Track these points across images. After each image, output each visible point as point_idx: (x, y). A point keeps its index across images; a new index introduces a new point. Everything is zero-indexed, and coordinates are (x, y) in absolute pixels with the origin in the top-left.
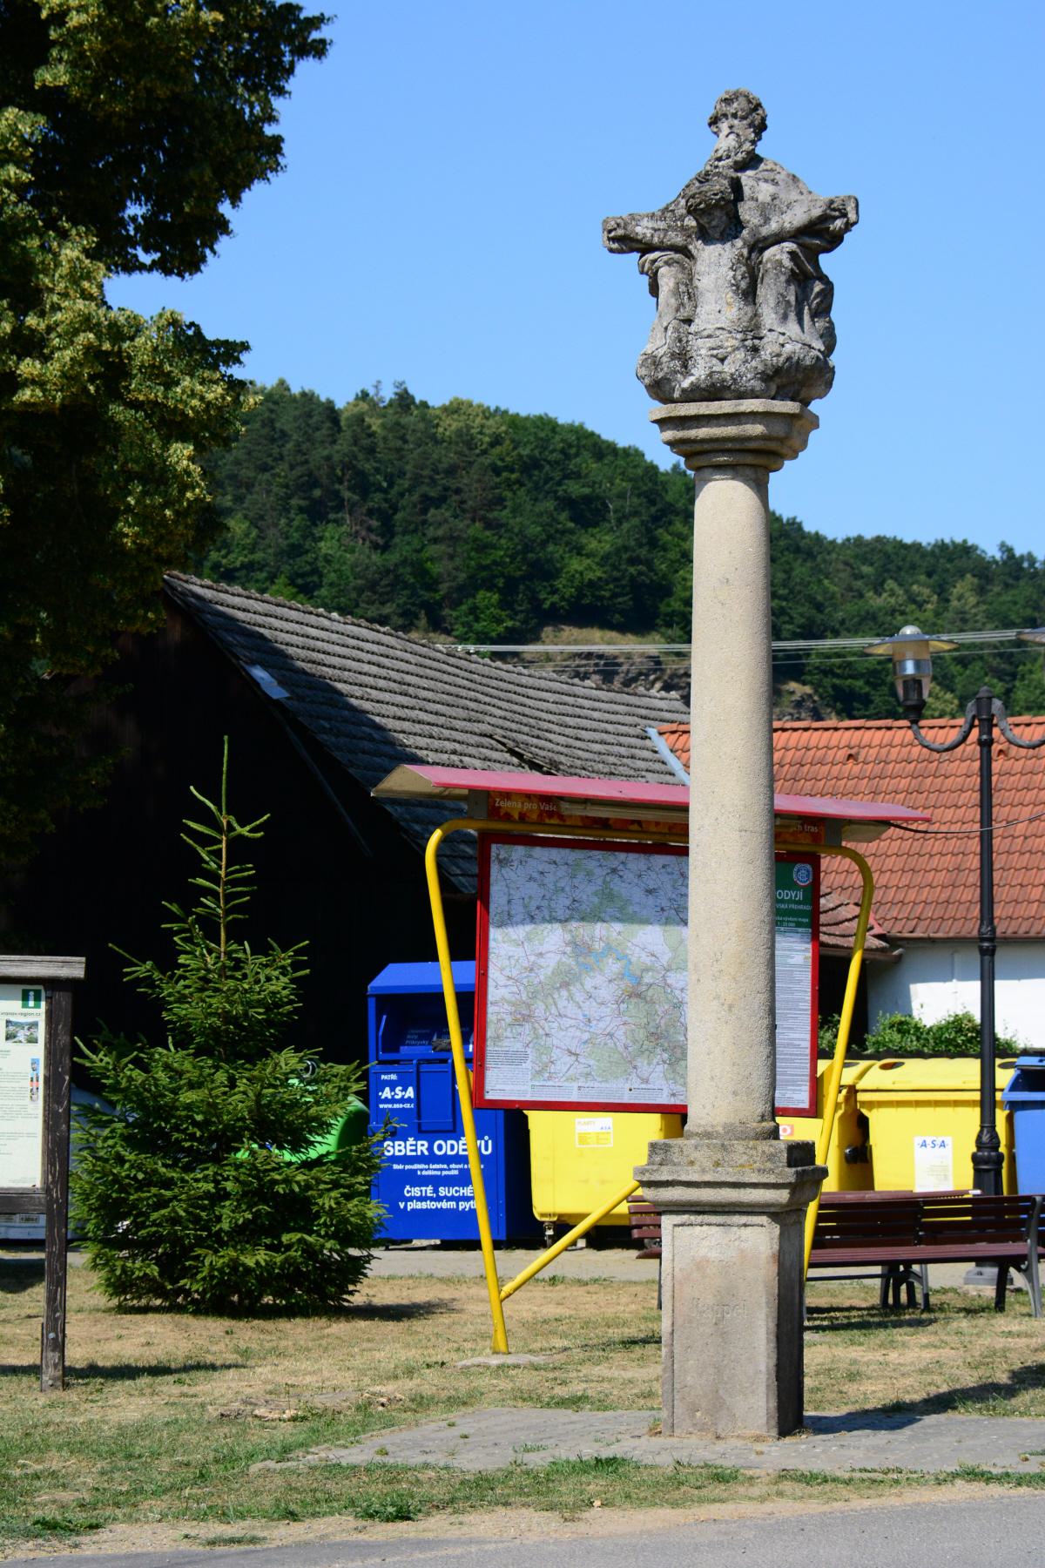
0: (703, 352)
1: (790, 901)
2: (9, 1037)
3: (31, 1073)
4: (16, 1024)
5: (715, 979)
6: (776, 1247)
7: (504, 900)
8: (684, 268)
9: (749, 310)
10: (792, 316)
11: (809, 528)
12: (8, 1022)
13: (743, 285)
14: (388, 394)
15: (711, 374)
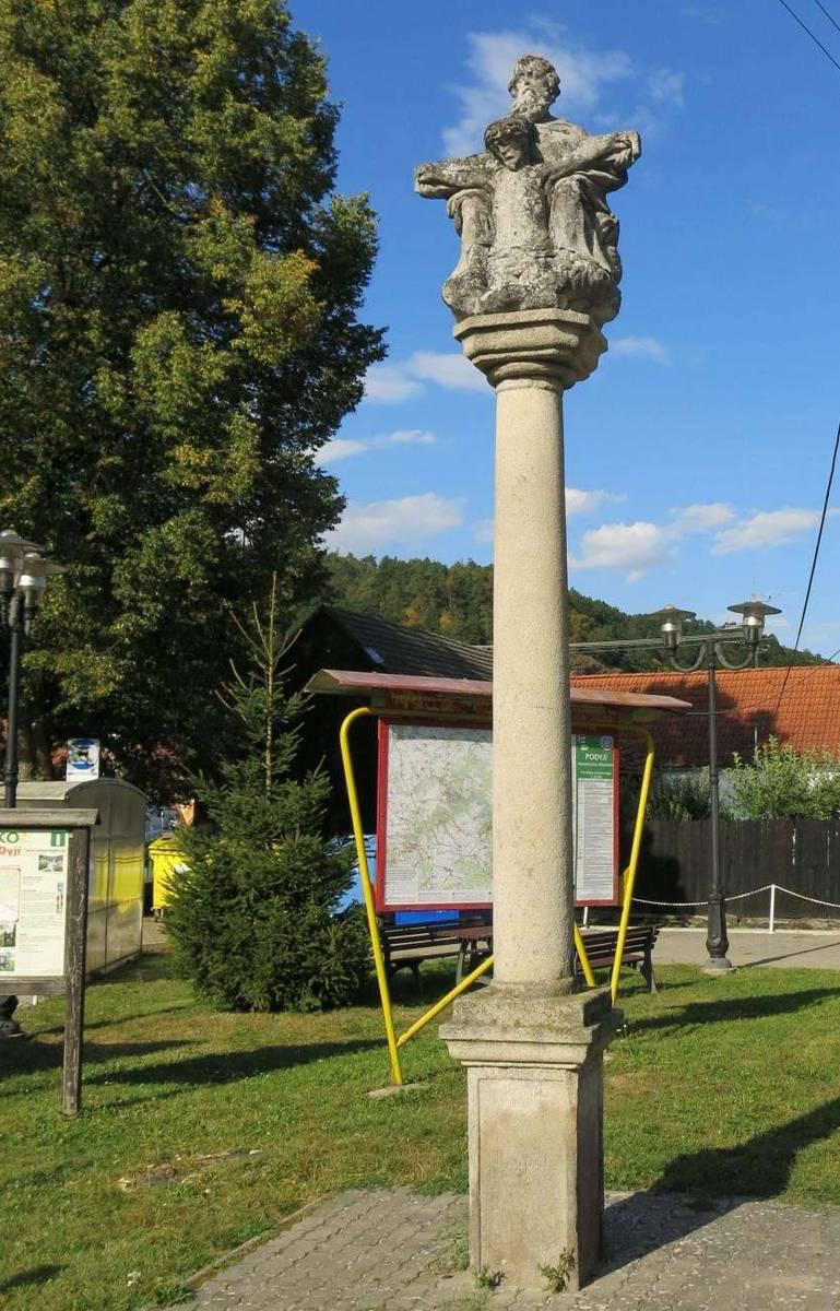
0: (500, 270)
1: (599, 761)
2: (40, 868)
3: (57, 894)
4: (47, 858)
5: (515, 845)
6: (575, 1102)
7: (397, 764)
8: (484, 201)
9: (543, 233)
10: (581, 238)
11: (621, 611)
12: (41, 857)
13: (537, 209)
14: (465, 563)
15: (506, 287)
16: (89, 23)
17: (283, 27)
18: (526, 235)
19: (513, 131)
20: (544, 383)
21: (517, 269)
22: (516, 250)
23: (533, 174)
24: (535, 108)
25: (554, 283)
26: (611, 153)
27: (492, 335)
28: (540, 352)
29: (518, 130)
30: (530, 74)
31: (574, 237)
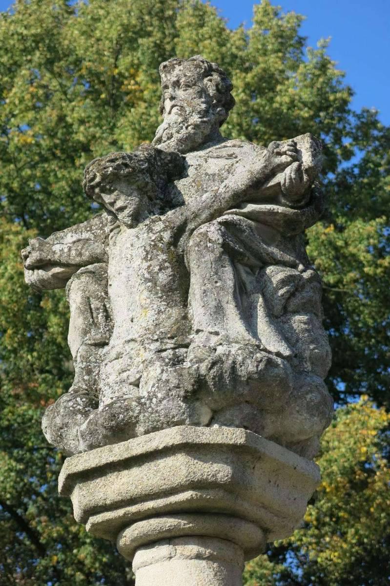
9: (175, 312)
10: (231, 309)
13: (163, 278)
16: (76, 151)
17: (343, 107)
18: (147, 318)
19: (118, 168)
20: (193, 549)
21: (133, 375)
22: (132, 345)
23: (159, 226)
24: (184, 131)
25: (178, 387)
26: (273, 173)
27: (100, 481)
28: (173, 499)
29: (126, 165)
30: (177, 84)
31: (219, 311)
